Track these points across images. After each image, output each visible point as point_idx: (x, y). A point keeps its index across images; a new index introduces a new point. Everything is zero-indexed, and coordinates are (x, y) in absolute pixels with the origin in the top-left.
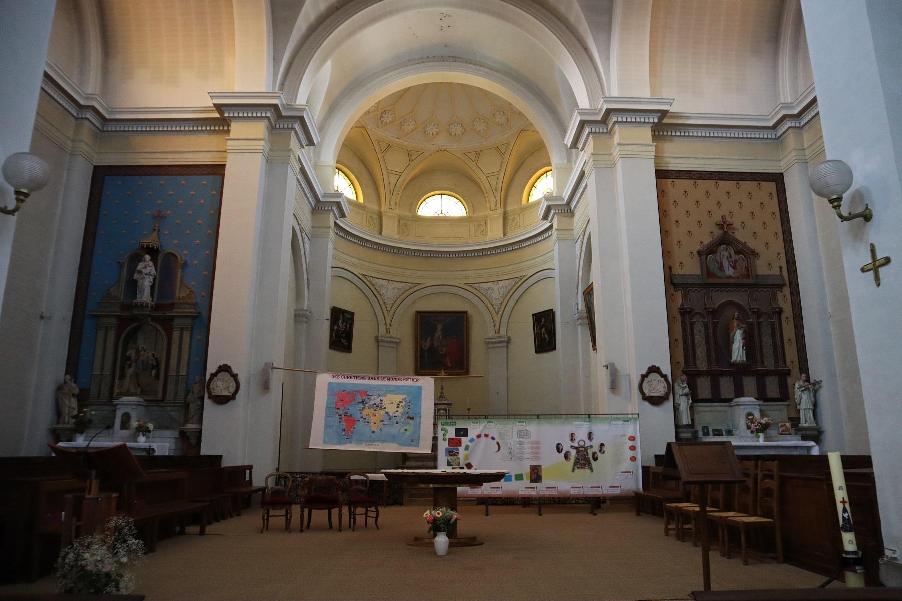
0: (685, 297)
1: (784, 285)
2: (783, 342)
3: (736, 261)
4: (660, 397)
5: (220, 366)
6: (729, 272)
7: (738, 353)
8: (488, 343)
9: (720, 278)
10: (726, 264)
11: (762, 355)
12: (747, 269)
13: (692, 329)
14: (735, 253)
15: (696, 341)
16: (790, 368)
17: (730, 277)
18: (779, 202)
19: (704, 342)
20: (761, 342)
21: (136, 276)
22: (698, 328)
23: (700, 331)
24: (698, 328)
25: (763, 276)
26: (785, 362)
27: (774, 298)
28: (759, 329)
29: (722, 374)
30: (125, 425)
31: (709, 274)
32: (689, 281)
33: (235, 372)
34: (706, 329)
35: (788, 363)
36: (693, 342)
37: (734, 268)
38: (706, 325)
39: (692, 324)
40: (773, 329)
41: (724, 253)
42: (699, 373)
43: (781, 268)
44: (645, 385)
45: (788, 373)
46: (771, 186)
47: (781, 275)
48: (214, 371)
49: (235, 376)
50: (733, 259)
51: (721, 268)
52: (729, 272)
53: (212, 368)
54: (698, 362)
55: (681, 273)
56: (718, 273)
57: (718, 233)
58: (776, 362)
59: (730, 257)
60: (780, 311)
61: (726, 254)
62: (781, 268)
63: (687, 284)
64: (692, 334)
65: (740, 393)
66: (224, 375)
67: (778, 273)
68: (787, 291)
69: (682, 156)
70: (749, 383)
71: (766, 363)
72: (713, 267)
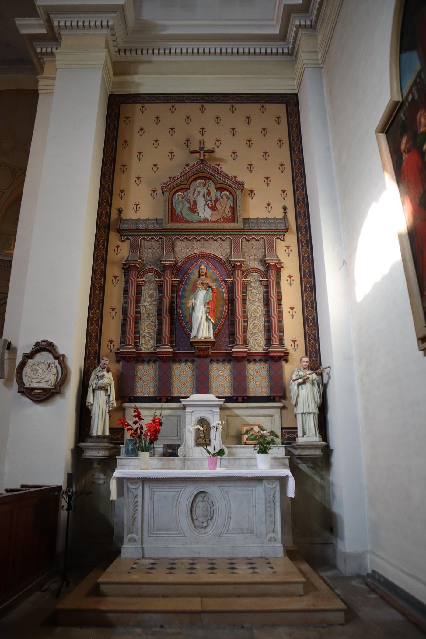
0: (135, 248)
1: (287, 230)
2: (280, 312)
3: (217, 200)
4: (44, 390)
5: (37, 344)
7: (203, 329)
10: (201, 203)
11: (245, 332)
13: (138, 293)
15: (143, 310)
16: (290, 350)
17: (206, 220)
19: (155, 312)
20: (245, 312)
22: (149, 293)
23: (151, 296)
24: (149, 293)
26: (282, 342)
27: (272, 247)
28: (244, 292)
29: (176, 358)
30: (203, 439)
32: (142, 226)
33: (61, 351)
34: (161, 292)
35: (287, 343)
36: (138, 312)
37: (214, 208)
38: (160, 287)
39: (139, 287)
40: (267, 293)
41: (199, 192)
42: (140, 358)
43: (285, 209)
44: (27, 370)
45: (285, 357)
47: (285, 218)
48: (28, 351)
49: (60, 359)
50: (213, 197)
51: (193, 209)
53: (24, 346)
54: (142, 341)
55: (134, 216)
56: (187, 215)
58: (269, 341)
59: (209, 193)
60: (278, 268)
61: (204, 191)
62: (285, 209)
63: (138, 230)
64: (138, 302)
65: (202, 386)
66: (44, 357)
68: (291, 239)
70: (221, 375)
71: (251, 342)
72: (182, 208)
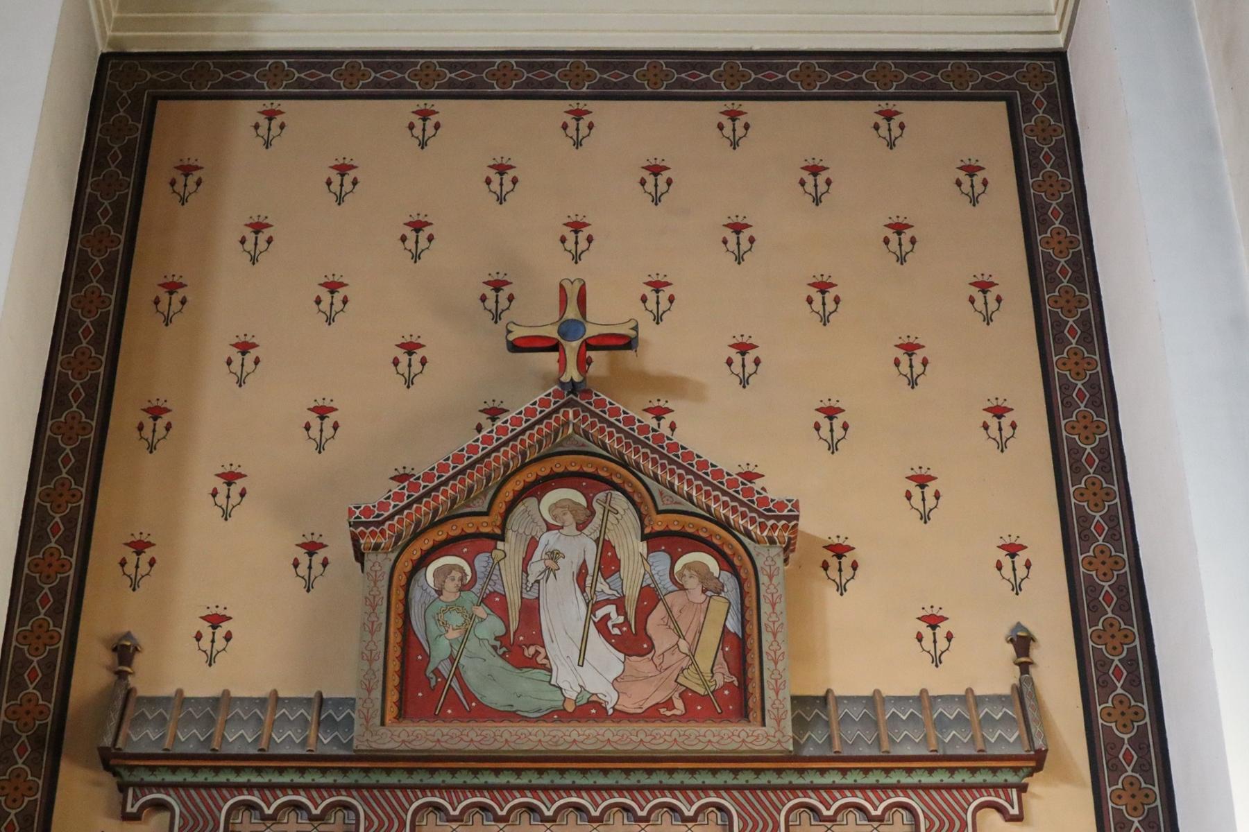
1: (1038, 760)
3: (650, 597)
6: (583, 665)
8: (402, 705)
9: (511, 716)
10: (564, 614)
12: (740, 650)
14: (653, 539)
18: (1032, 219)
21: (570, 708)
25: (873, 701)
31: (413, 680)
37: (632, 642)
41: (557, 551)
43: (1022, 643)
46: (981, 129)
47: (1024, 697)
50: (631, 578)
51: (522, 646)
52: (583, 665)
55: (199, 682)
56: (519, 689)
57: (527, 386)
59: (609, 562)
61: (579, 548)
62: (1022, 643)
63: (216, 759)
67: (996, 677)
69: (392, 711)
72: (458, 637)
